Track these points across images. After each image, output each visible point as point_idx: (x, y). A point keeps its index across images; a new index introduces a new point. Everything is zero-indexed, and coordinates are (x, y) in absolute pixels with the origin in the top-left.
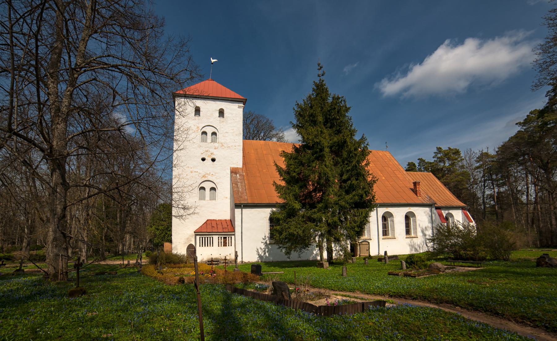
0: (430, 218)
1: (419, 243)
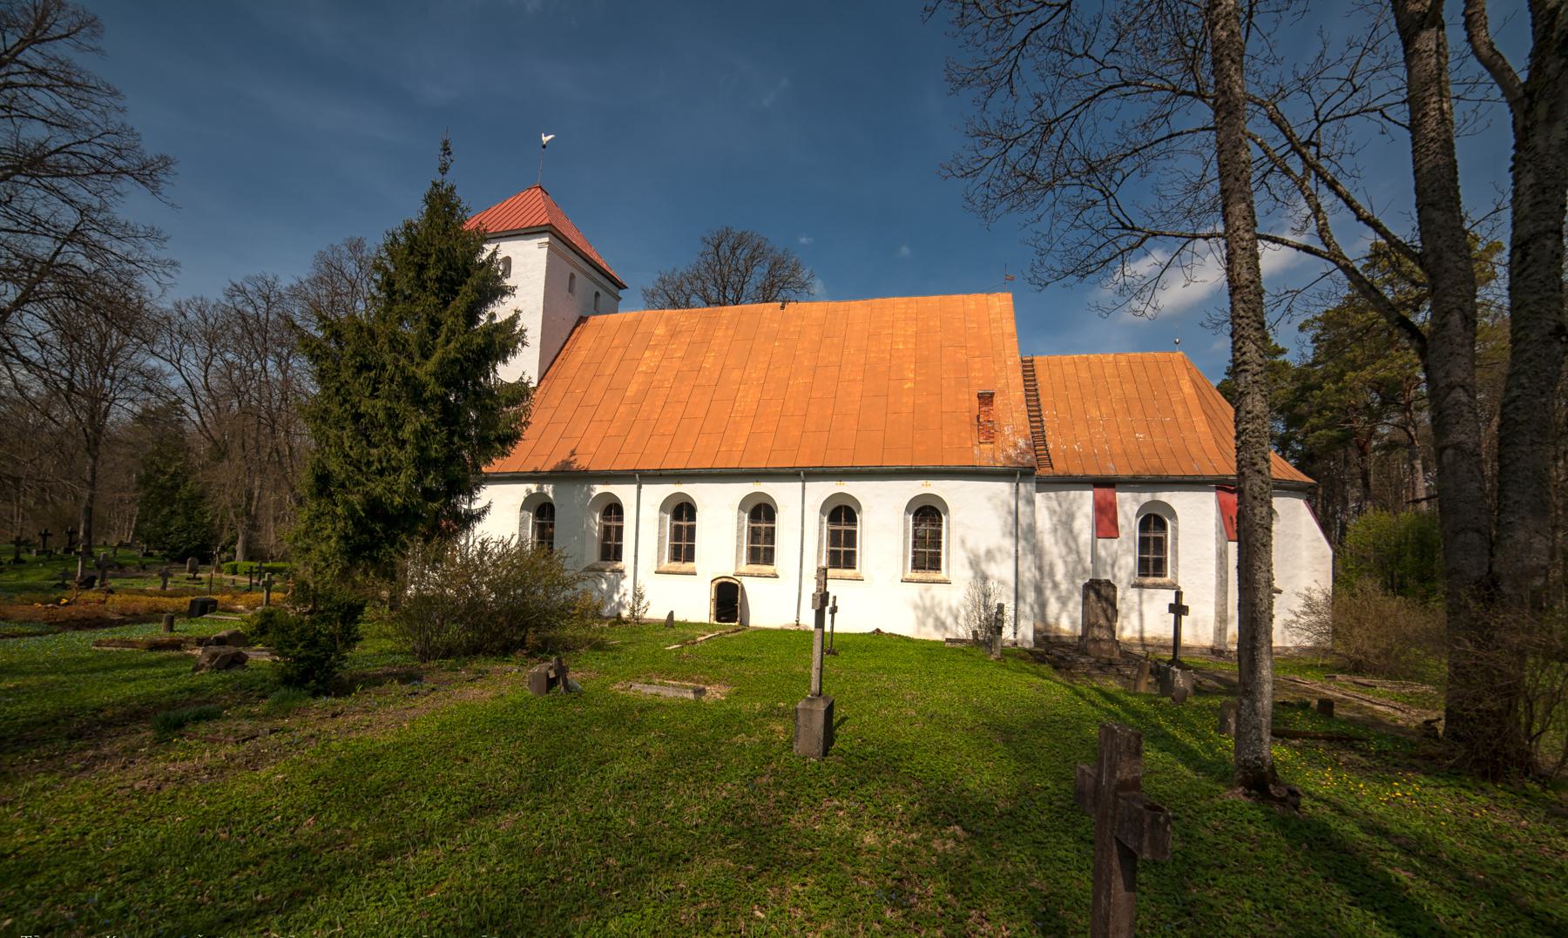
0: (1011, 520)
1: (954, 604)
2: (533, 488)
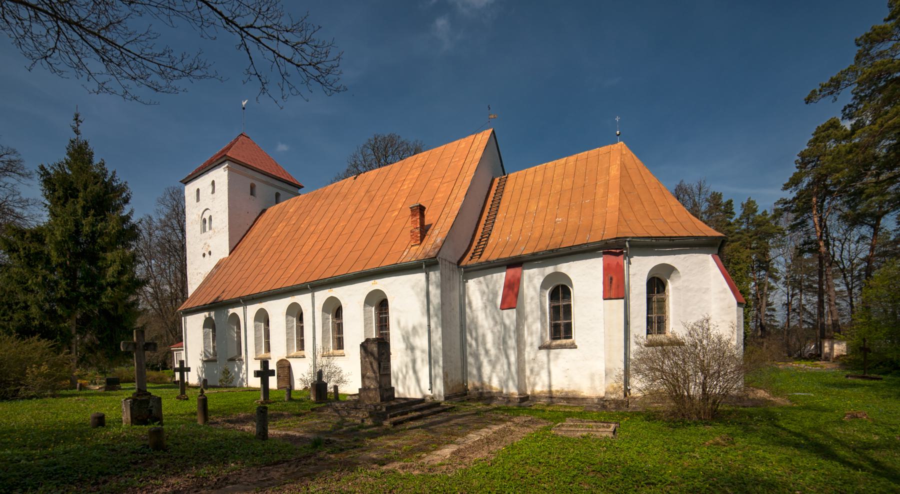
2: (207, 314)
